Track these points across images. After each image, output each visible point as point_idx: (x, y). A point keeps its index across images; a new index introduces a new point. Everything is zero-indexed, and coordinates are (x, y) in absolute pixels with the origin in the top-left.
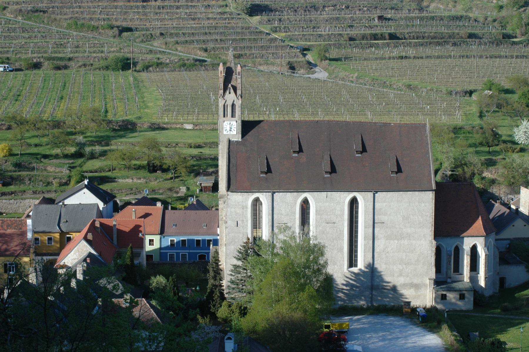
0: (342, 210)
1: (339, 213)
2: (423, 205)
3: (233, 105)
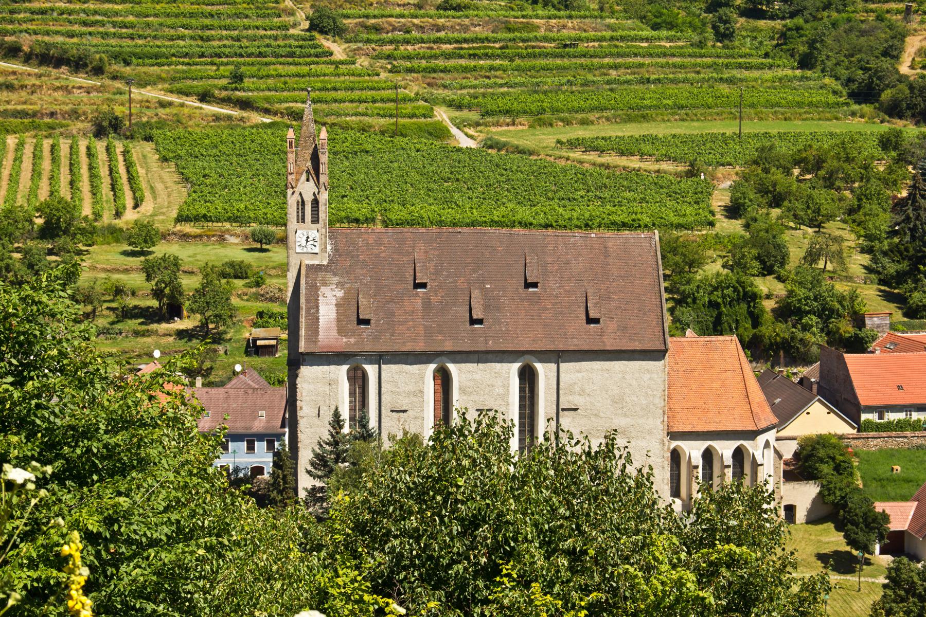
0: (506, 387)
1: (501, 391)
2: (647, 376)
3: (315, 202)
